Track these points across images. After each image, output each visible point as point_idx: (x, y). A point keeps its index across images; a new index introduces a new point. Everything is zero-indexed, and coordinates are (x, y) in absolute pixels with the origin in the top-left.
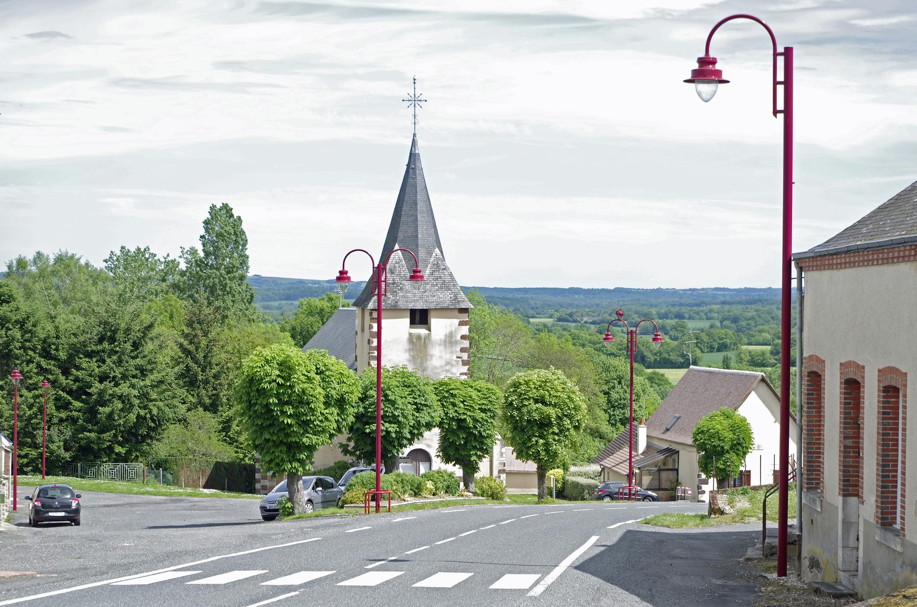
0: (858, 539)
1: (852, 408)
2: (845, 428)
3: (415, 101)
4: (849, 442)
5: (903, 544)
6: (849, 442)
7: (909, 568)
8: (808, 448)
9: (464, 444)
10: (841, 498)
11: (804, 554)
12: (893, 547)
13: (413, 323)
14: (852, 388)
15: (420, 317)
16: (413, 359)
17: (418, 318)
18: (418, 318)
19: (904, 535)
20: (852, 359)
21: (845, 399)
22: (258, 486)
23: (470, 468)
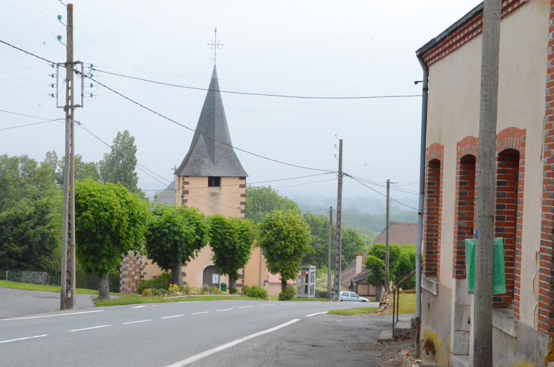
0: (469, 322)
1: (467, 188)
2: (460, 209)
3: (216, 44)
4: (464, 223)
5: (516, 328)
6: (464, 223)
7: (524, 356)
8: (428, 235)
9: (229, 259)
10: (454, 280)
11: (422, 337)
12: (505, 330)
13: (210, 185)
14: (468, 163)
15: (214, 182)
16: (491, 316)
17: (213, 183)
18: (213, 183)
19: (518, 317)
20: (468, 134)
21: (461, 178)
22: (121, 288)
23: (233, 277)
